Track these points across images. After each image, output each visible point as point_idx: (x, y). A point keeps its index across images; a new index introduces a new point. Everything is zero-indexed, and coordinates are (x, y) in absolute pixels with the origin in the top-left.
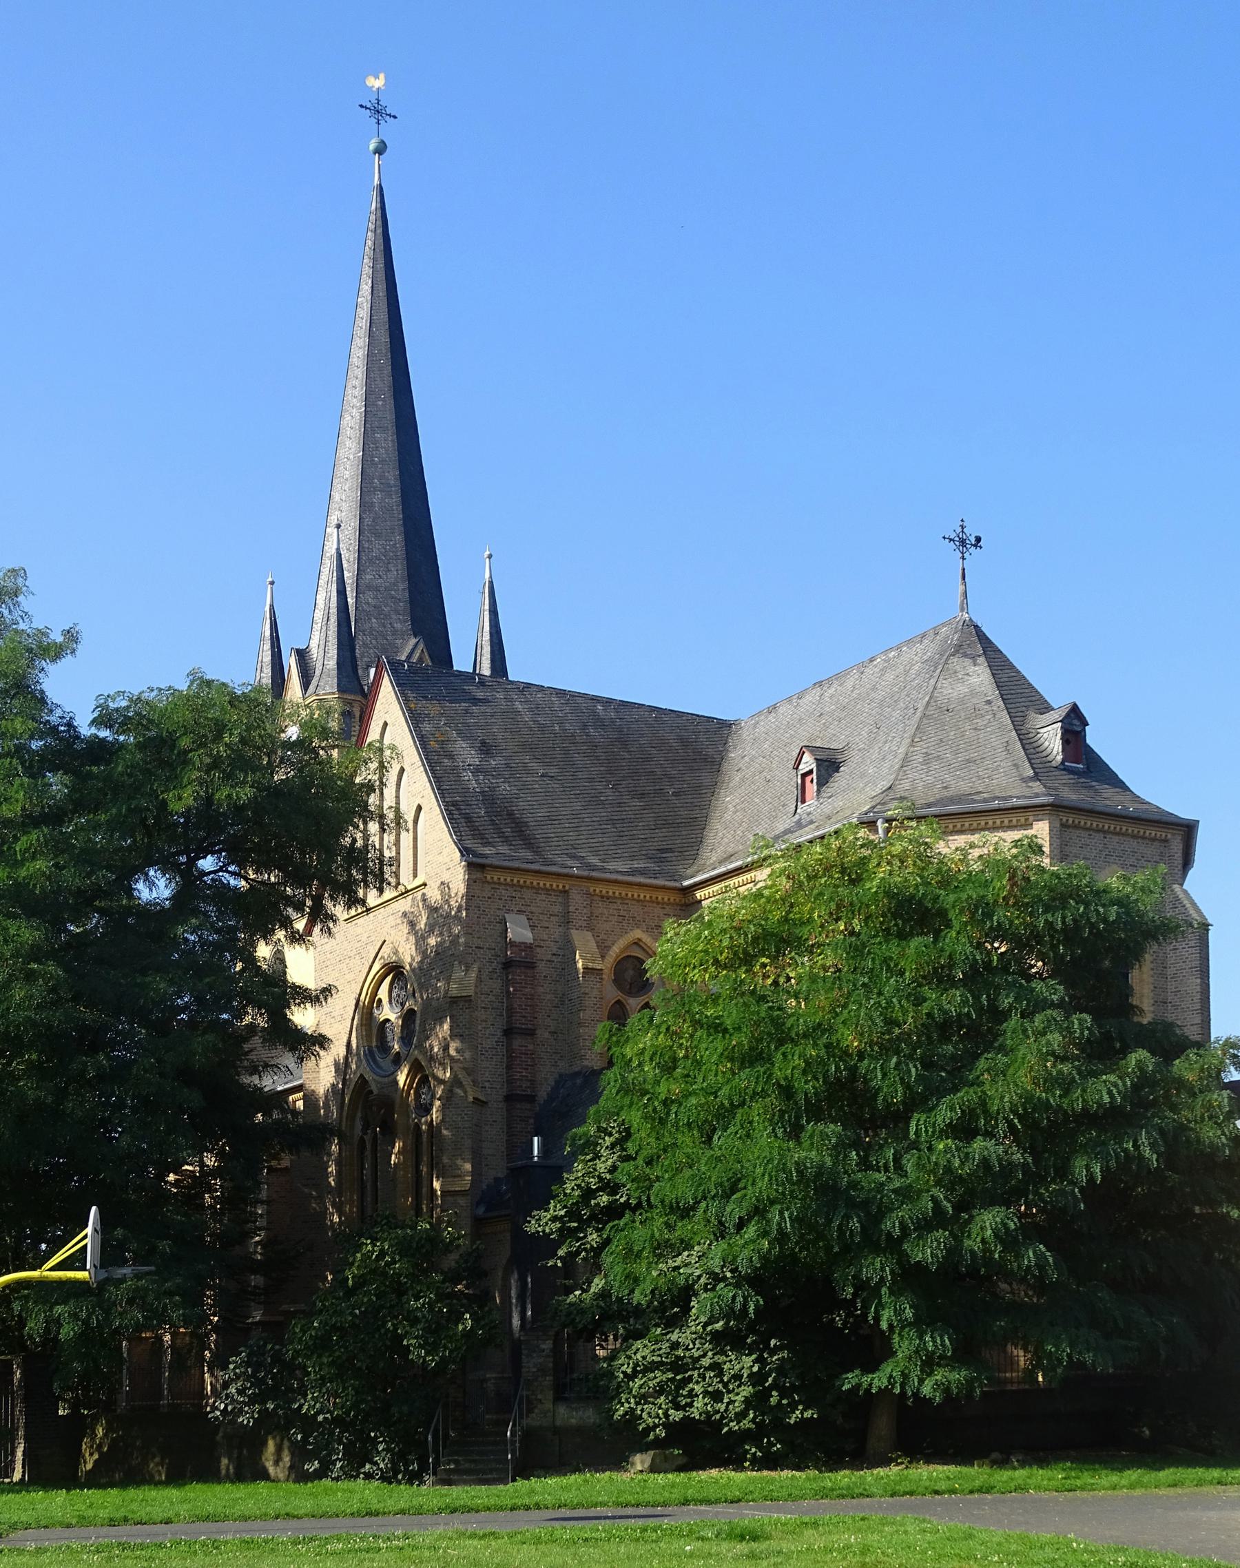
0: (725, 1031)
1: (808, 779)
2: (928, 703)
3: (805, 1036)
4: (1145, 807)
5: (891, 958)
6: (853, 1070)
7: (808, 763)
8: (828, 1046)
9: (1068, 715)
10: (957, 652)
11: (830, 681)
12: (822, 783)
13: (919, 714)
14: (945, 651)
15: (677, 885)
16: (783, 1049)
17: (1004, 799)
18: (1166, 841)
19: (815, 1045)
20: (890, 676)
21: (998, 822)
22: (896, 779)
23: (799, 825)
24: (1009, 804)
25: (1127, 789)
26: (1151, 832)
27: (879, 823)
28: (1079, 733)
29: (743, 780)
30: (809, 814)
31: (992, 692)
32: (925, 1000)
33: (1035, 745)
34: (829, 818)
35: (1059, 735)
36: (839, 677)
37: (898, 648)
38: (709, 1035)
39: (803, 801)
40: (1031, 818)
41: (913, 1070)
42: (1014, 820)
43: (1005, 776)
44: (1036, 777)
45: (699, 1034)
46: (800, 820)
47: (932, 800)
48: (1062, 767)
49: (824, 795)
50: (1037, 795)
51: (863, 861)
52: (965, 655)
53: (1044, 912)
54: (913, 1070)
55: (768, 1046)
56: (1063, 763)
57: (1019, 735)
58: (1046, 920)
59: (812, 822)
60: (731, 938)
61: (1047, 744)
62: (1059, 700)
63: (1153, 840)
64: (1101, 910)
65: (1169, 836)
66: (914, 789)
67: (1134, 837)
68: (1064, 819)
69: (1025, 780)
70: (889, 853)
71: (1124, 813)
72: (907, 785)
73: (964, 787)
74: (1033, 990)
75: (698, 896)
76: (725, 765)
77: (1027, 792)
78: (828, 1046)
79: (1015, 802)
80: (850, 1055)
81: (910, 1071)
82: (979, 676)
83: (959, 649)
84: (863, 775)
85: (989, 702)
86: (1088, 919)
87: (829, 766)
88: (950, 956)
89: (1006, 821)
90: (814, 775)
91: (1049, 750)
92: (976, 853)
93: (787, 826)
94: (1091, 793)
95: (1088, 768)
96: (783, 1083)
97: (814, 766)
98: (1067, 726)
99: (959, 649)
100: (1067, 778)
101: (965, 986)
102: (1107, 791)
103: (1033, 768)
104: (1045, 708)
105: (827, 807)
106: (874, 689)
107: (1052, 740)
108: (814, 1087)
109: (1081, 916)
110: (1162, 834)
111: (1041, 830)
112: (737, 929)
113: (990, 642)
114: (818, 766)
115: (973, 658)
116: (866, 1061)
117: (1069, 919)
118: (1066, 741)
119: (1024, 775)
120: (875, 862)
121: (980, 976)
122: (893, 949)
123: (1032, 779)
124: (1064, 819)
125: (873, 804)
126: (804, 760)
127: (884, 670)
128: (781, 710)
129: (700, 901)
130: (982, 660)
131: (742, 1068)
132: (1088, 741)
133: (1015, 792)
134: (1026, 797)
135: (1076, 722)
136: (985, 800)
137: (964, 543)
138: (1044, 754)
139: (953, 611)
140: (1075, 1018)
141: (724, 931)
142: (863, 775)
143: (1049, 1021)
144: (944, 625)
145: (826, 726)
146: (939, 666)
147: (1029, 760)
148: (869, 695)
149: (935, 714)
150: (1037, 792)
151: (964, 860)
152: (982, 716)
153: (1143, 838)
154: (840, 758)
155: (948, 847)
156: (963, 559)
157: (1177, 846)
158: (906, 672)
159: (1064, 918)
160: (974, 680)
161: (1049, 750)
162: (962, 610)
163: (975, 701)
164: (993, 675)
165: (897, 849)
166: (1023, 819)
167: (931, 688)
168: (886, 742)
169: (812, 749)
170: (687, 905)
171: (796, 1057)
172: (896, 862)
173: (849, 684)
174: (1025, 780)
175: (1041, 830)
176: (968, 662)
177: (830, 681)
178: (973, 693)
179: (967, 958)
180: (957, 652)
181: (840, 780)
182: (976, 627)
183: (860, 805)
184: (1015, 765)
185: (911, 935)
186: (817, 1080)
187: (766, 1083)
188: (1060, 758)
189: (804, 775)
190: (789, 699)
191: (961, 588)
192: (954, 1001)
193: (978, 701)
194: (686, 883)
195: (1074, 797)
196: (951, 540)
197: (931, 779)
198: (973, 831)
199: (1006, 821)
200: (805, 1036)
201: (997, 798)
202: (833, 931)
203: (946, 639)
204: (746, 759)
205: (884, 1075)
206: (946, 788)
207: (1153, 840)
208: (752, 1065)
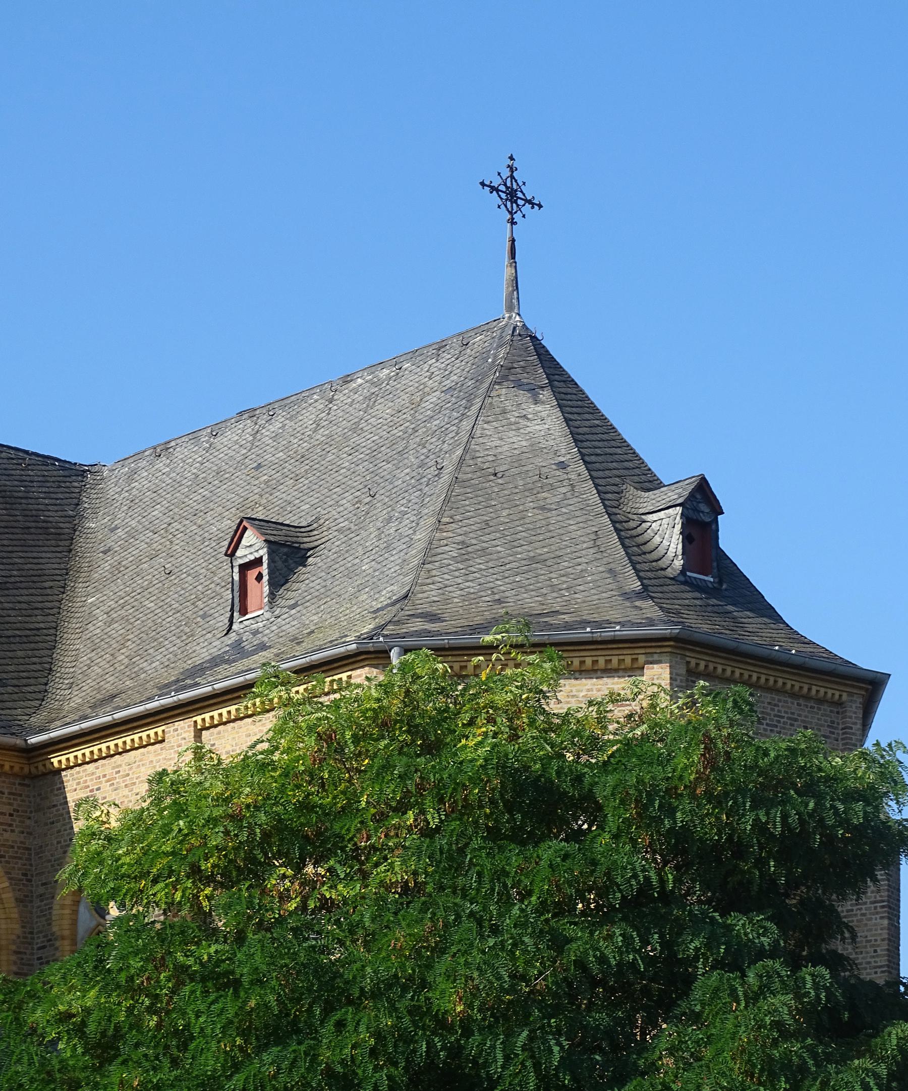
0: (236, 984)
1: (252, 574)
2: (461, 460)
3: (376, 995)
5: (507, 874)
6: (455, 1052)
7: (253, 545)
8: (413, 1011)
9: (692, 495)
11: (270, 409)
12: (279, 581)
13: (446, 478)
14: (485, 375)
15: (19, 742)
16: (337, 1016)
17: (598, 625)
18: (840, 704)
19: (393, 1009)
20: (384, 410)
21: (589, 661)
22: (414, 583)
23: (239, 650)
24: (607, 634)
26: (819, 689)
27: (394, 653)
28: (708, 524)
29: (117, 569)
30: (256, 633)
31: (567, 450)
32: (569, 941)
33: (640, 540)
35: (678, 527)
36: (288, 403)
37: (396, 363)
38: (206, 993)
39: (244, 611)
40: (642, 659)
41: (556, 1049)
42: (615, 660)
43: (594, 589)
44: (645, 592)
45: (187, 989)
46: (239, 642)
47: (478, 620)
48: (682, 579)
50: (651, 622)
51: (444, 716)
52: (519, 385)
53: (752, 808)
54: (556, 1049)
55: (310, 1011)
56: (683, 572)
57: (614, 522)
58: (757, 820)
59: (263, 647)
60: (227, 833)
61: (657, 539)
62: (674, 467)
63: (821, 701)
64: (841, 807)
65: (845, 697)
66: (447, 601)
67: (794, 695)
68: (693, 662)
70: (492, 705)
71: (784, 657)
72: (433, 593)
74: (729, 928)
75: (55, 761)
76: (81, 543)
77: (634, 616)
78: (413, 1011)
79: (618, 631)
80: (450, 1029)
81: (551, 1051)
83: (507, 374)
85: (562, 466)
86: (822, 820)
87: (289, 554)
88: (608, 874)
89: (602, 661)
90: (264, 569)
92: (619, 712)
93: (215, 652)
94: (728, 623)
96: (339, 1069)
97: (263, 552)
98: (691, 514)
99: (507, 374)
100: (689, 597)
101: (624, 919)
102: (752, 622)
103: (640, 578)
104: (651, 483)
105: (289, 623)
106: (356, 428)
107: (667, 534)
108: (389, 1077)
109: (811, 815)
110: (832, 692)
111: (658, 675)
112: (236, 818)
113: (558, 366)
114: (270, 554)
115: (533, 390)
116: (477, 1037)
117: (793, 819)
118: (687, 538)
119: (627, 589)
120: (466, 718)
121: (644, 906)
122: (514, 858)
123: (639, 595)
124: (693, 662)
125: (380, 621)
126: (244, 542)
127: (371, 400)
128: (180, 453)
129: (59, 771)
131: (261, 1049)
133: (613, 615)
134: (633, 624)
135: (704, 507)
136: (568, 626)
137: (511, 195)
138: (654, 556)
139: (492, 307)
140: (807, 973)
141: (212, 821)
142: (351, 574)
143: (769, 977)
144: (478, 330)
145: (271, 487)
147: (633, 564)
149: (472, 480)
150: (649, 616)
151: (602, 721)
152: (552, 488)
153: (807, 698)
154: (306, 541)
155: (574, 695)
156: (513, 222)
157: (854, 709)
158: (416, 406)
159: (785, 817)
160: (535, 427)
162: (510, 308)
163: (539, 461)
164: (567, 420)
165: (502, 698)
166: (628, 660)
168: (389, 520)
169: (262, 525)
170: (32, 777)
171: (362, 1028)
172: (502, 720)
173: (308, 417)
175: (658, 675)
176: (523, 396)
177: (270, 409)
178: (535, 449)
179: (635, 876)
181: (309, 579)
182: (534, 338)
183: (352, 623)
184: (611, 571)
185: (542, 839)
186: (395, 1064)
187: (308, 1070)
188: (679, 563)
189: (245, 568)
190: (194, 436)
191: (508, 272)
192: (611, 944)
193: (544, 462)
194: (34, 740)
195: (705, 628)
196: (529, 202)
197: (473, 587)
198: (609, 672)
199: (602, 661)
200: (376, 995)
201: (585, 623)
202: (397, 827)
205: (507, 1058)
206: (499, 601)
207: (821, 701)
208: (281, 1041)
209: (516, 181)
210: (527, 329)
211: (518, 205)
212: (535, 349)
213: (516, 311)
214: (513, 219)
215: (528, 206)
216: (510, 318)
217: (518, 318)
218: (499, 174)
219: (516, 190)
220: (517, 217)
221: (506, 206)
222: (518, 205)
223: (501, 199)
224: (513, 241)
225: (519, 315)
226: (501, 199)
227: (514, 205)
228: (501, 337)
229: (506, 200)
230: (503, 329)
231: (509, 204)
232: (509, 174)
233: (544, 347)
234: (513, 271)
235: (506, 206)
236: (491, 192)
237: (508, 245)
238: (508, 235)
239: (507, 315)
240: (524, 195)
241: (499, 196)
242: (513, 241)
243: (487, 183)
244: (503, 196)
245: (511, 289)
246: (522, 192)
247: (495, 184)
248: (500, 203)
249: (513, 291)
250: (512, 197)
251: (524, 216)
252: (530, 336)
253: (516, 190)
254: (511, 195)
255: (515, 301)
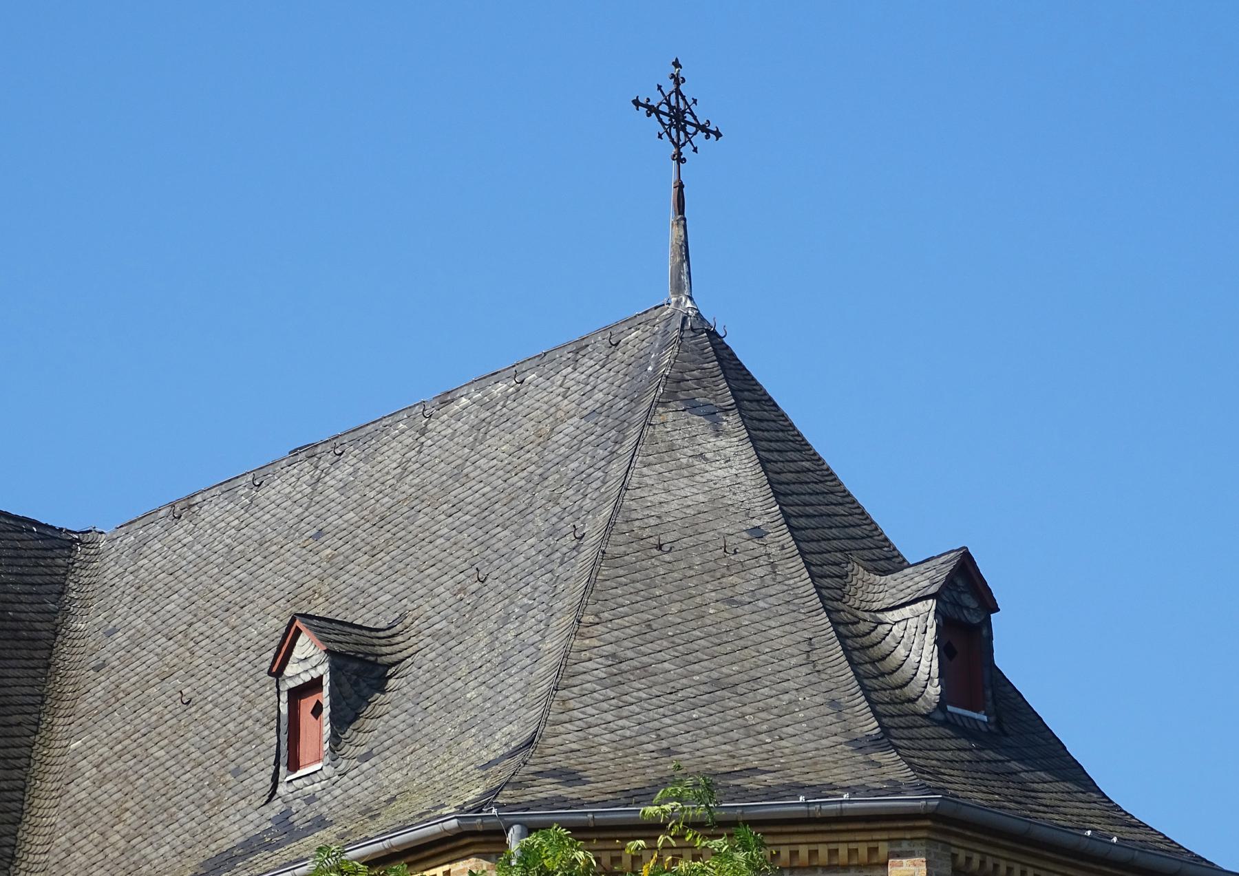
1: (307, 705)
2: (611, 524)
4: (1139, 836)
7: (309, 659)
9: (950, 581)
10: (671, 396)
11: (337, 446)
12: (346, 715)
14: (643, 392)
17: (816, 791)
20: (499, 445)
22: (543, 720)
25: (1088, 784)
29: (114, 694)
30: (310, 799)
31: (765, 511)
34: (370, 813)
35: (932, 632)
37: (516, 373)
39: (294, 765)
40: (884, 849)
42: (843, 850)
44: (885, 739)
46: (285, 816)
48: (940, 717)
49: (349, 750)
50: (895, 788)
56: (941, 706)
57: (835, 624)
59: (321, 823)
61: (901, 652)
66: (591, 750)
68: (962, 855)
69: (860, 744)
73: (714, 753)
76: (64, 655)
77: (870, 777)
79: (846, 802)
82: (727, 465)
83: (675, 390)
84: (450, 705)
85: (757, 533)
87: (361, 672)
90: (325, 697)
91: (907, 670)
95: (998, 723)
97: (323, 669)
99: (675, 390)
102: (1050, 790)
103: (877, 715)
104: (888, 561)
106: (458, 475)
107: (913, 641)
114: (333, 671)
115: (712, 415)
119: (858, 732)
126: (297, 653)
128: (209, 512)
130: (731, 421)
132: (999, 661)
133: (840, 775)
136: (771, 793)
137: (677, 119)
138: (898, 678)
142: (450, 705)
144: (631, 322)
145: (337, 566)
146: (627, 425)
148: (445, 491)
149: (626, 556)
156: (679, 159)
158: (544, 439)
160: (717, 472)
161: (907, 670)
162: (678, 288)
163: (723, 527)
164: (763, 462)
166: (863, 850)
167: (614, 486)
168: (506, 620)
169: (323, 626)
173: (390, 457)
174: (860, 744)
176: (699, 424)
177: (337, 446)
178: (718, 507)
180: (671, 396)
181: (391, 712)
182: (712, 334)
184: (832, 703)
188: (934, 691)
189: (297, 694)
190: (228, 486)
191: (675, 233)
195: (978, 797)
196: (703, 128)
203: (641, 361)
204: (120, 637)
206: (668, 751)
209: (683, 98)
210: (703, 319)
211: (686, 134)
212: (715, 350)
213: (687, 292)
214: (680, 154)
215: (701, 134)
216: (678, 303)
217: (689, 304)
218: (659, 87)
219: (684, 112)
220: (686, 151)
221: (670, 135)
222: (686, 134)
223: (663, 124)
224: (680, 186)
225: (691, 299)
226: (663, 124)
227: (682, 133)
228: (666, 333)
229: (670, 126)
230: (668, 320)
231: (674, 131)
232: (673, 87)
233: (728, 347)
234: (682, 233)
235: (670, 135)
236: (649, 115)
237: (673, 193)
238: (674, 178)
239: (674, 299)
240: (695, 118)
241: (660, 120)
242: (680, 186)
243: (643, 101)
244: (666, 119)
245: (678, 259)
246: (692, 113)
247: (654, 103)
248: (662, 130)
249: (682, 262)
250: (678, 121)
251: (695, 150)
252: (707, 331)
253: (684, 112)
254: (677, 119)
255: (684, 278)
